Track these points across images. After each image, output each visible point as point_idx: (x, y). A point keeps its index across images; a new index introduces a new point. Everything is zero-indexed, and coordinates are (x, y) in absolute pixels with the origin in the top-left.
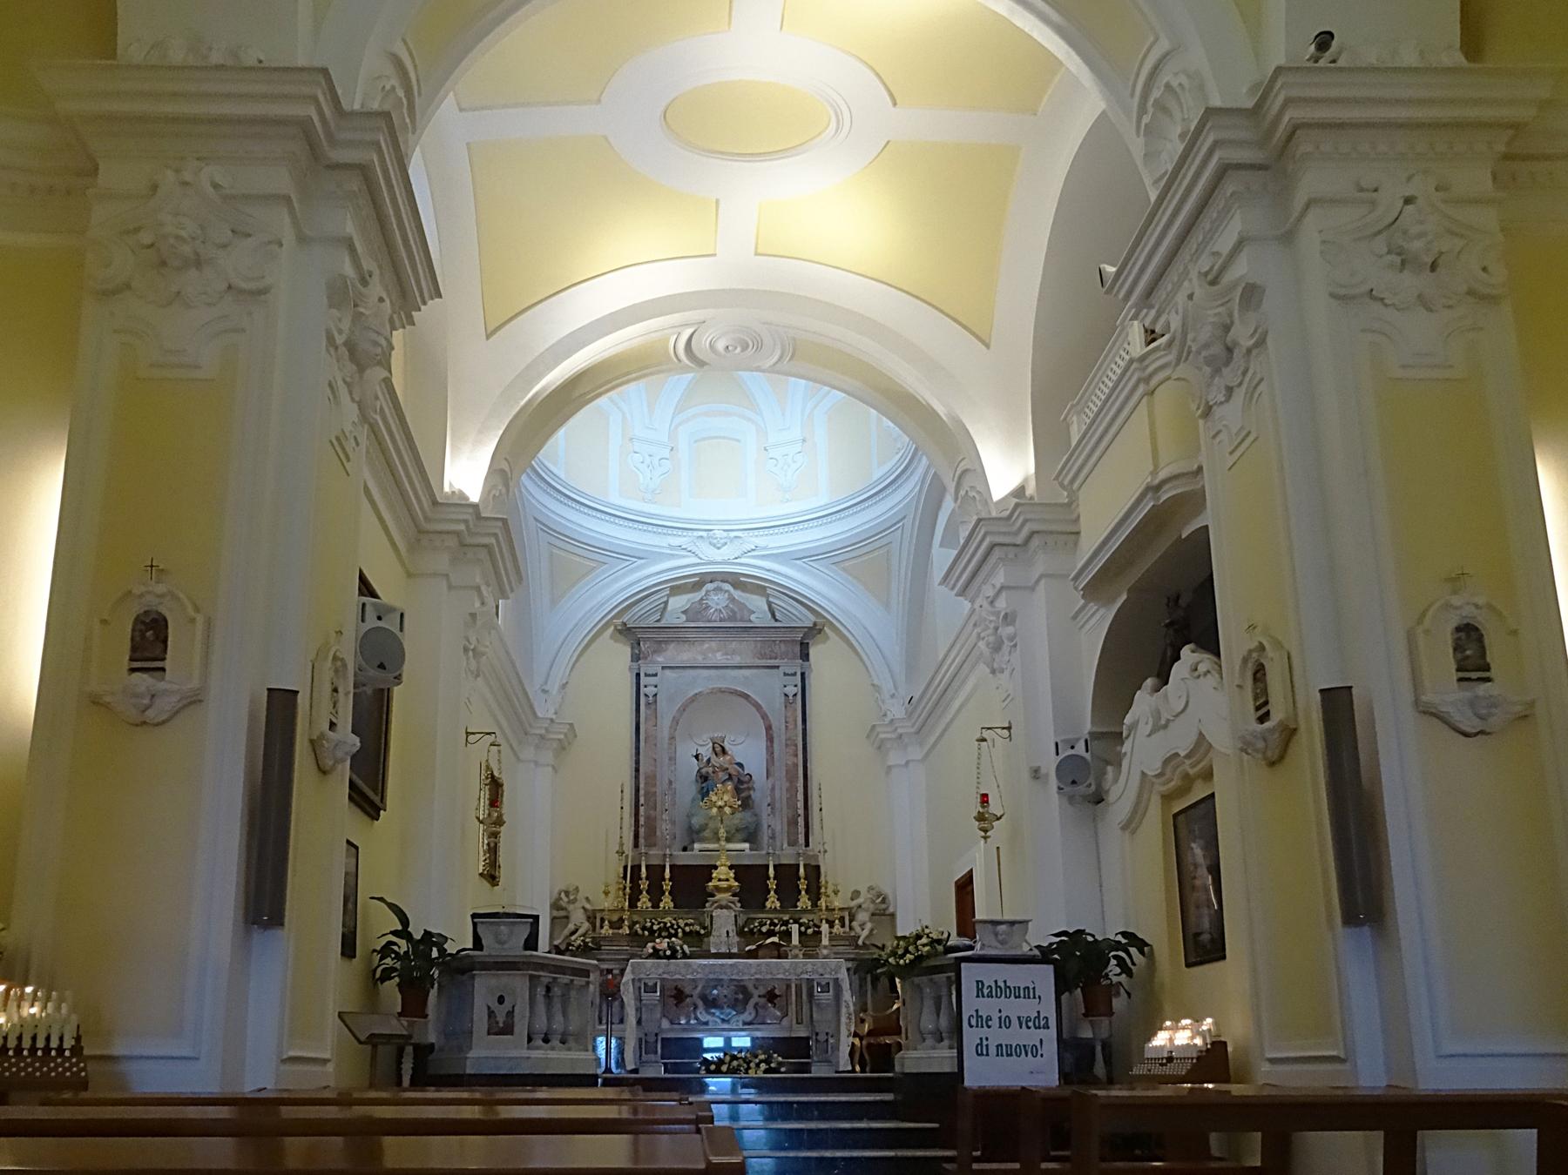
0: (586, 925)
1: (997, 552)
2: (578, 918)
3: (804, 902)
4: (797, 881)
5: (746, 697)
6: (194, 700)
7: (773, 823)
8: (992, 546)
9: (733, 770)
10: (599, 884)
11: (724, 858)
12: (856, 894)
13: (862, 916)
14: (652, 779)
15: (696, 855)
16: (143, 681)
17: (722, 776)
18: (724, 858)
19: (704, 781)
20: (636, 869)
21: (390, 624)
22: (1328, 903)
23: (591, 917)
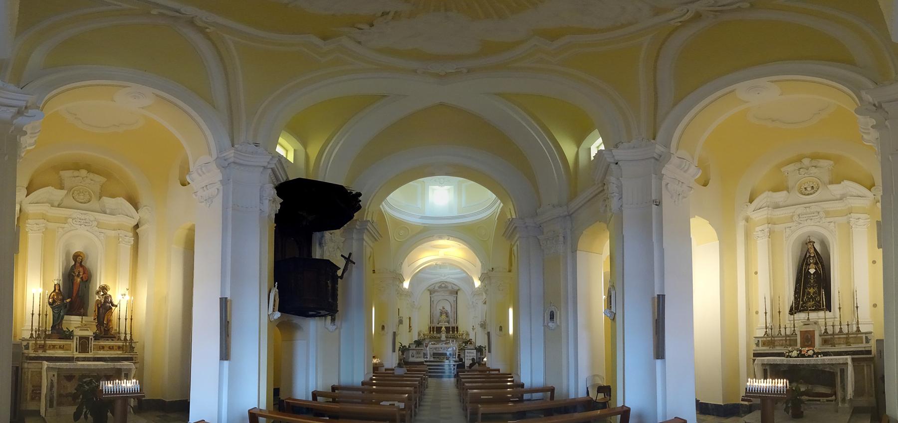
7: (452, 320)
11: (444, 325)
18: (444, 325)
19: (441, 314)
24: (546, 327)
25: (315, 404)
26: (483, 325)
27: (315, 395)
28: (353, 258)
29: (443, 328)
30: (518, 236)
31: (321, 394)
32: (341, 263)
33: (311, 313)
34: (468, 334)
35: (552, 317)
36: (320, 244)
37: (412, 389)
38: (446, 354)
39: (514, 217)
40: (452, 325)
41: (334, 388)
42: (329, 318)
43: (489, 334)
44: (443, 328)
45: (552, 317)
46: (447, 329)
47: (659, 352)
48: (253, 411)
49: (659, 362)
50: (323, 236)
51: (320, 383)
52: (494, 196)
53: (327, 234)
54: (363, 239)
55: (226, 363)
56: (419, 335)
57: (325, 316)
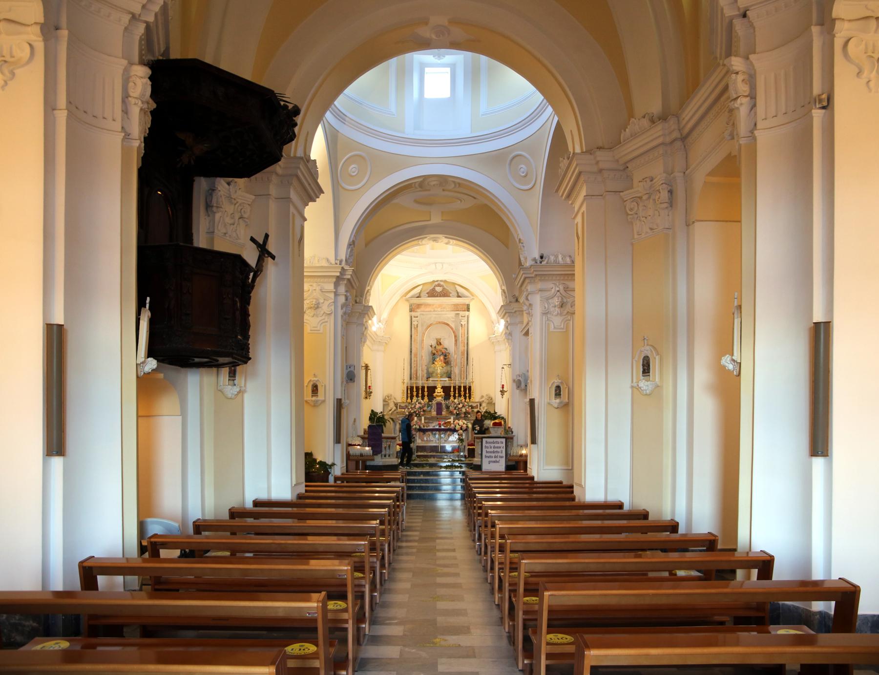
0: (394, 408)
1: (527, 281)
2: (392, 406)
3: (468, 400)
4: (467, 391)
5: (448, 325)
6: (324, 401)
7: (456, 371)
8: (525, 278)
9: (443, 350)
10: (399, 395)
11: (440, 383)
12: (482, 397)
13: (484, 405)
14: (416, 355)
15: (431, 383)
16: (314, 398)
17: (440, 353)
18: (440, 383)
19: (433, 356)
20: (412, 388)
21: (352, 369)
22: (526, 433)
23: (396, 405)
24: (635, 388)
25: (90, 599)
26: (521, 384)
27: (89, 572)
28: (271, 247)
29: (439, 391)
30: (583, 193)
31: (111, 569)
32: (251, 256)
33: (197, 360)
34: (491, 403)
35: (646, 369)
36: (208, 206)
37: (343, 567)
38: (443, 450)
39: (578, 150)
40: (457, 381)
41: (234, 514)
42: (225, 371)
43: (532, 402)
44: (439, 391)
45: (646, 369)
46: (446, 389)
47: (819, 442)
48: (85, 564)
49: (818, 463)
50: (212, 190)
51: (210, 503)
52: (539, 97)
53: (221, 184)
54: (288, 199)
55: (57, 462)
56: (386, 402)
57: (219, 366)
